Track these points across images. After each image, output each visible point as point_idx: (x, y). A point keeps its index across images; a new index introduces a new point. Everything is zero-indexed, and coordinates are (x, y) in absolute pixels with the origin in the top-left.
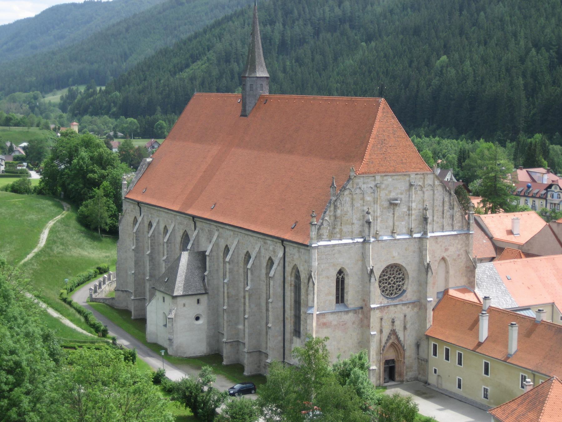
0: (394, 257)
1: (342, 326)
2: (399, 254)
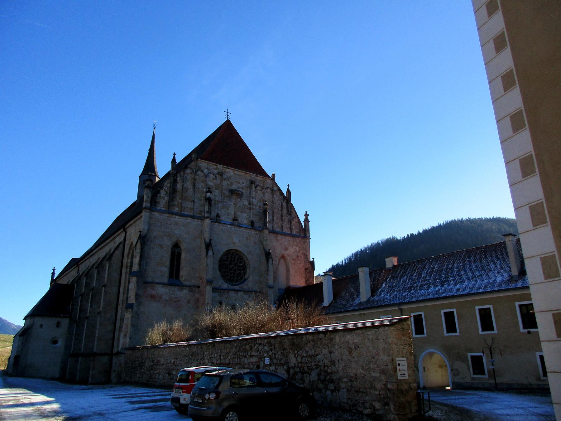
0: (235, 243)
1: (175, 302)
2: (240, 241)
